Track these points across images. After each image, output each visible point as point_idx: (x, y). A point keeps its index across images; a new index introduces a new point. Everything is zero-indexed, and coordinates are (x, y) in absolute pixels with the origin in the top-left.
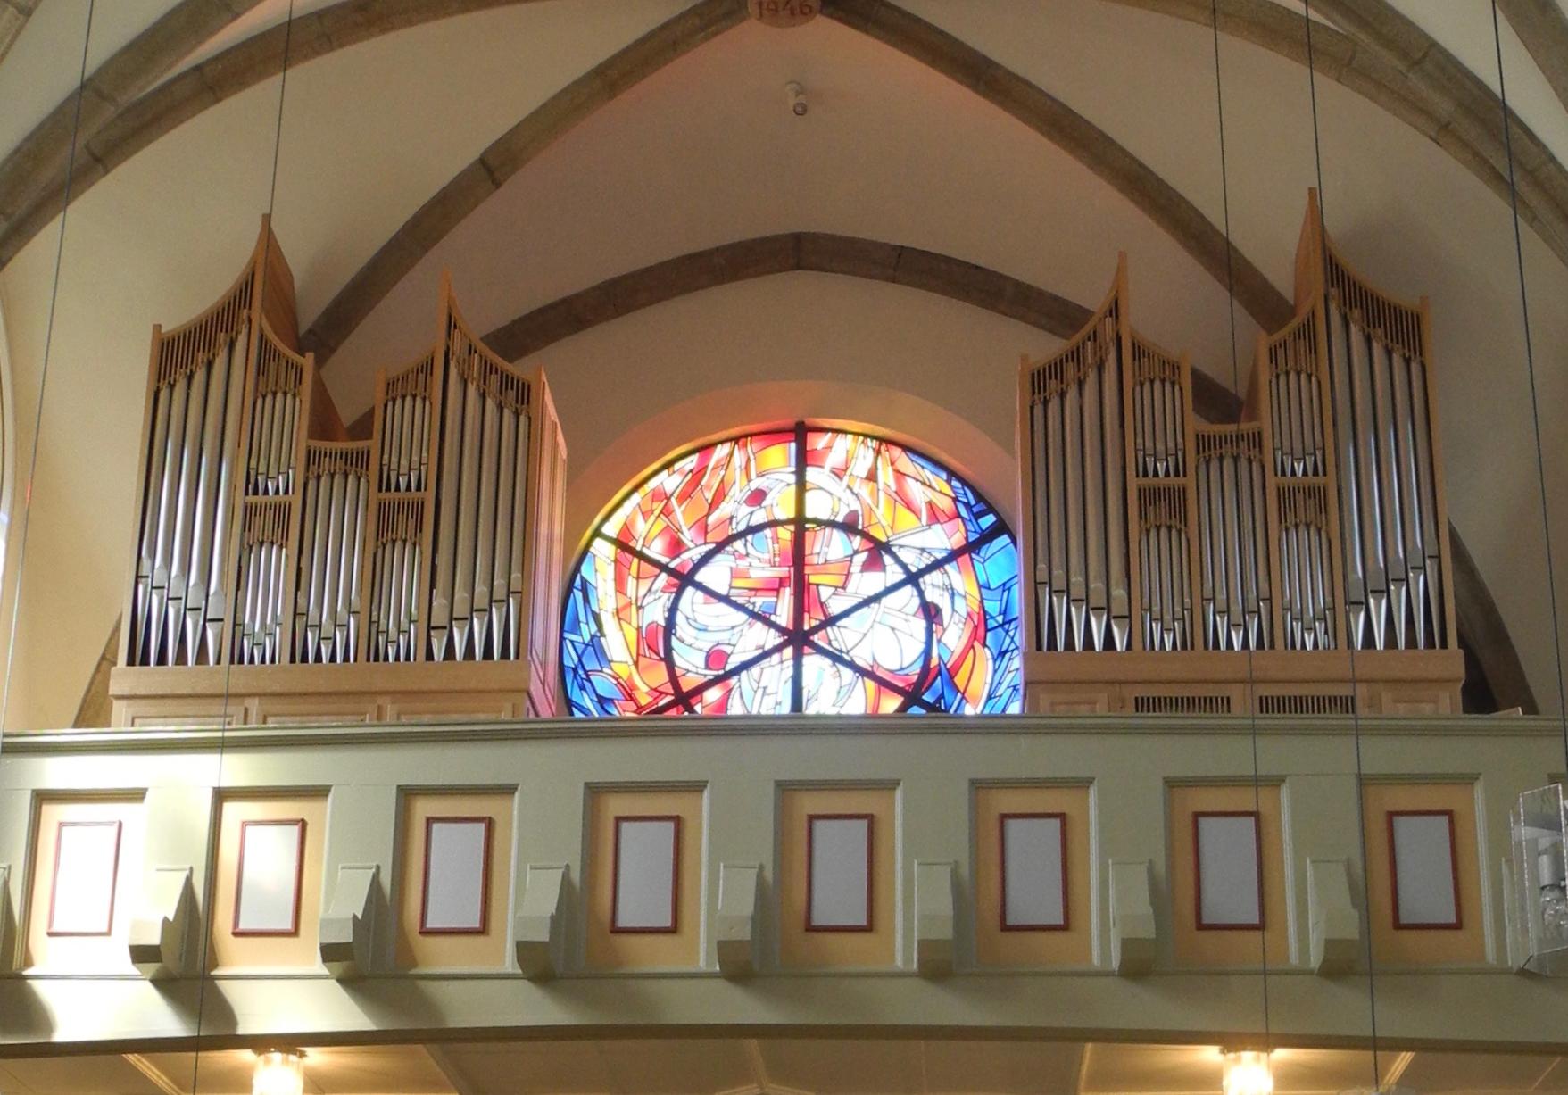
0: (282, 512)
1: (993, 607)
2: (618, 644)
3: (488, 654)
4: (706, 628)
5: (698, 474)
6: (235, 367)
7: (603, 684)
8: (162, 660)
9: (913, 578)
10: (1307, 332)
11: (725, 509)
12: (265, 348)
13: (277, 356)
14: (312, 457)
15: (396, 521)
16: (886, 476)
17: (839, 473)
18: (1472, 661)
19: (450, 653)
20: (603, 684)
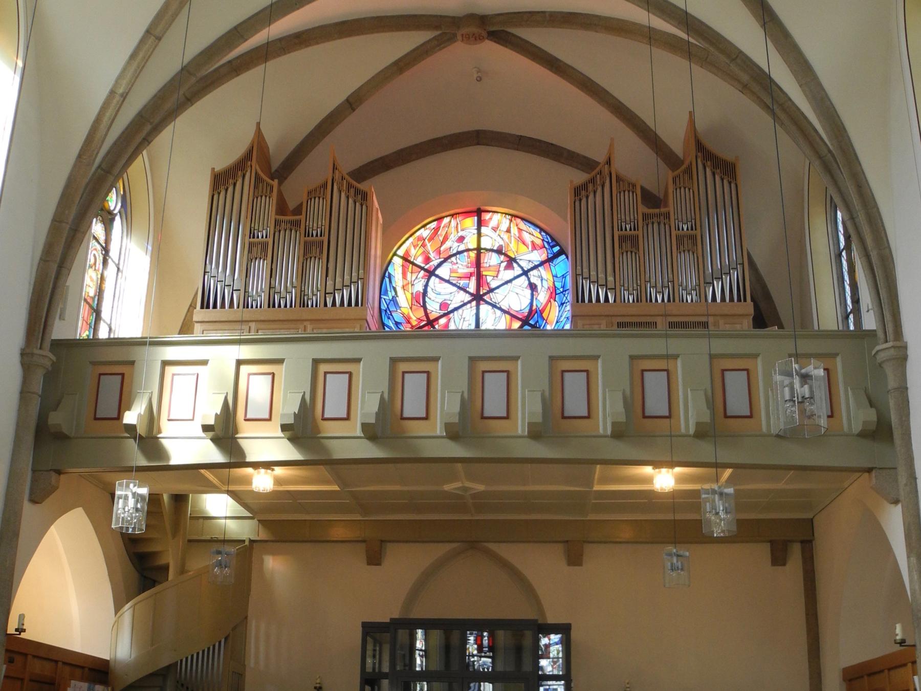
0: (264, 246)
1: (558, 285)
2: (404, 300)
3: (350, 304)
4: (440, 293)
5: (437, 230)
7: (397, 317)
8: (215, 307)
9: (525, 273)
10: (688, 171)
11: (448, 244)
12: (258, 179)
13: (263, 181)
14: (277, 223)
16: (514, 230)
17: (495, 229)
18: (756, 307)
20: (397, 317)
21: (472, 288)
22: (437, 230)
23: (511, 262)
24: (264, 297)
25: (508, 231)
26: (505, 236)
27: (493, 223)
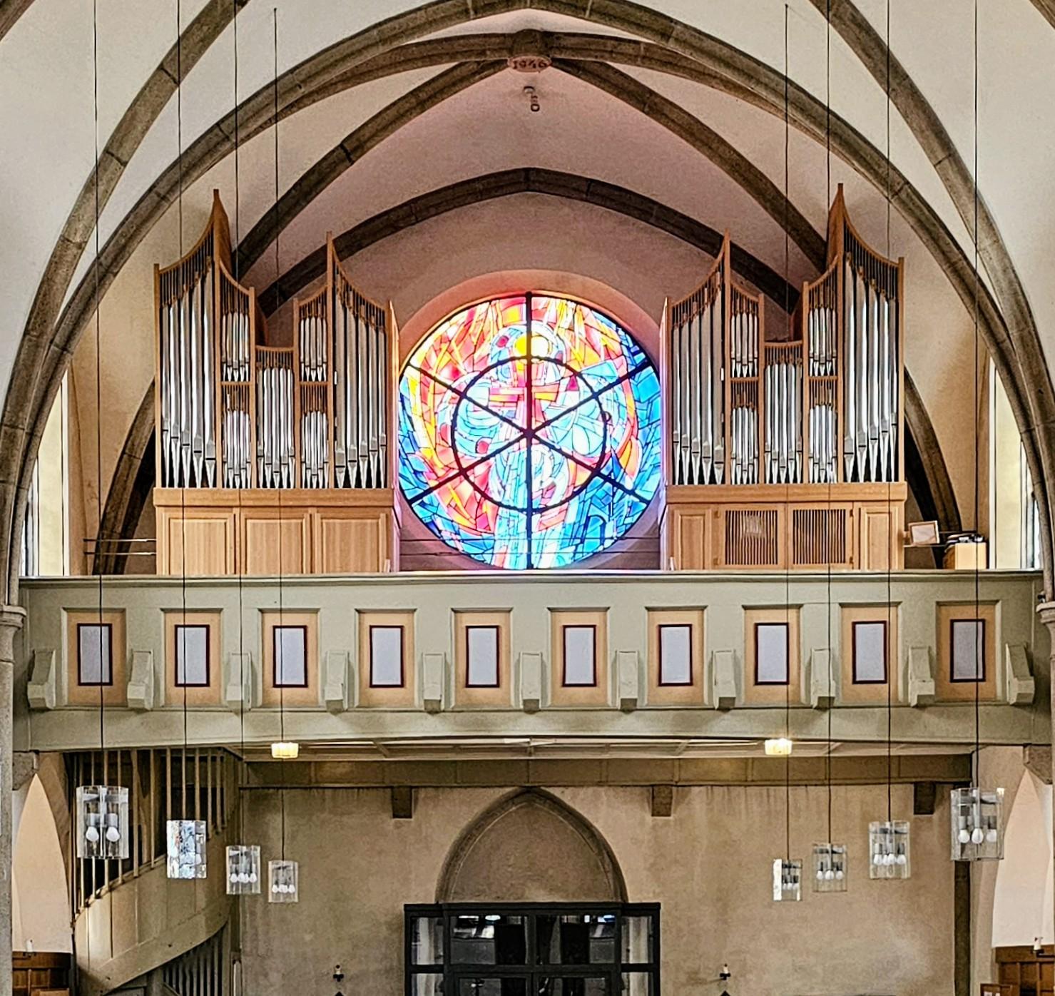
0: (242, 392)
2: (424, 436)
4: (483, 427)
5: (468, 324)
6: (208, 290)
10: (832, 282)
11: (483, 351)
15: (312, 398)
16: (580, 328)
19: (347, 484)
21: (521, 421)
22: (468, 324)
23: (577, 374)
24: (250, 473)
25: (571, 329)
26: (566, 336)
27: (549, 316)
